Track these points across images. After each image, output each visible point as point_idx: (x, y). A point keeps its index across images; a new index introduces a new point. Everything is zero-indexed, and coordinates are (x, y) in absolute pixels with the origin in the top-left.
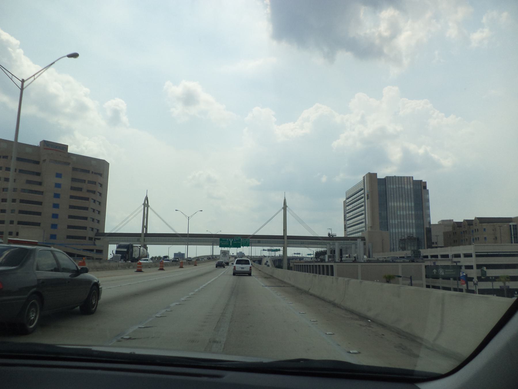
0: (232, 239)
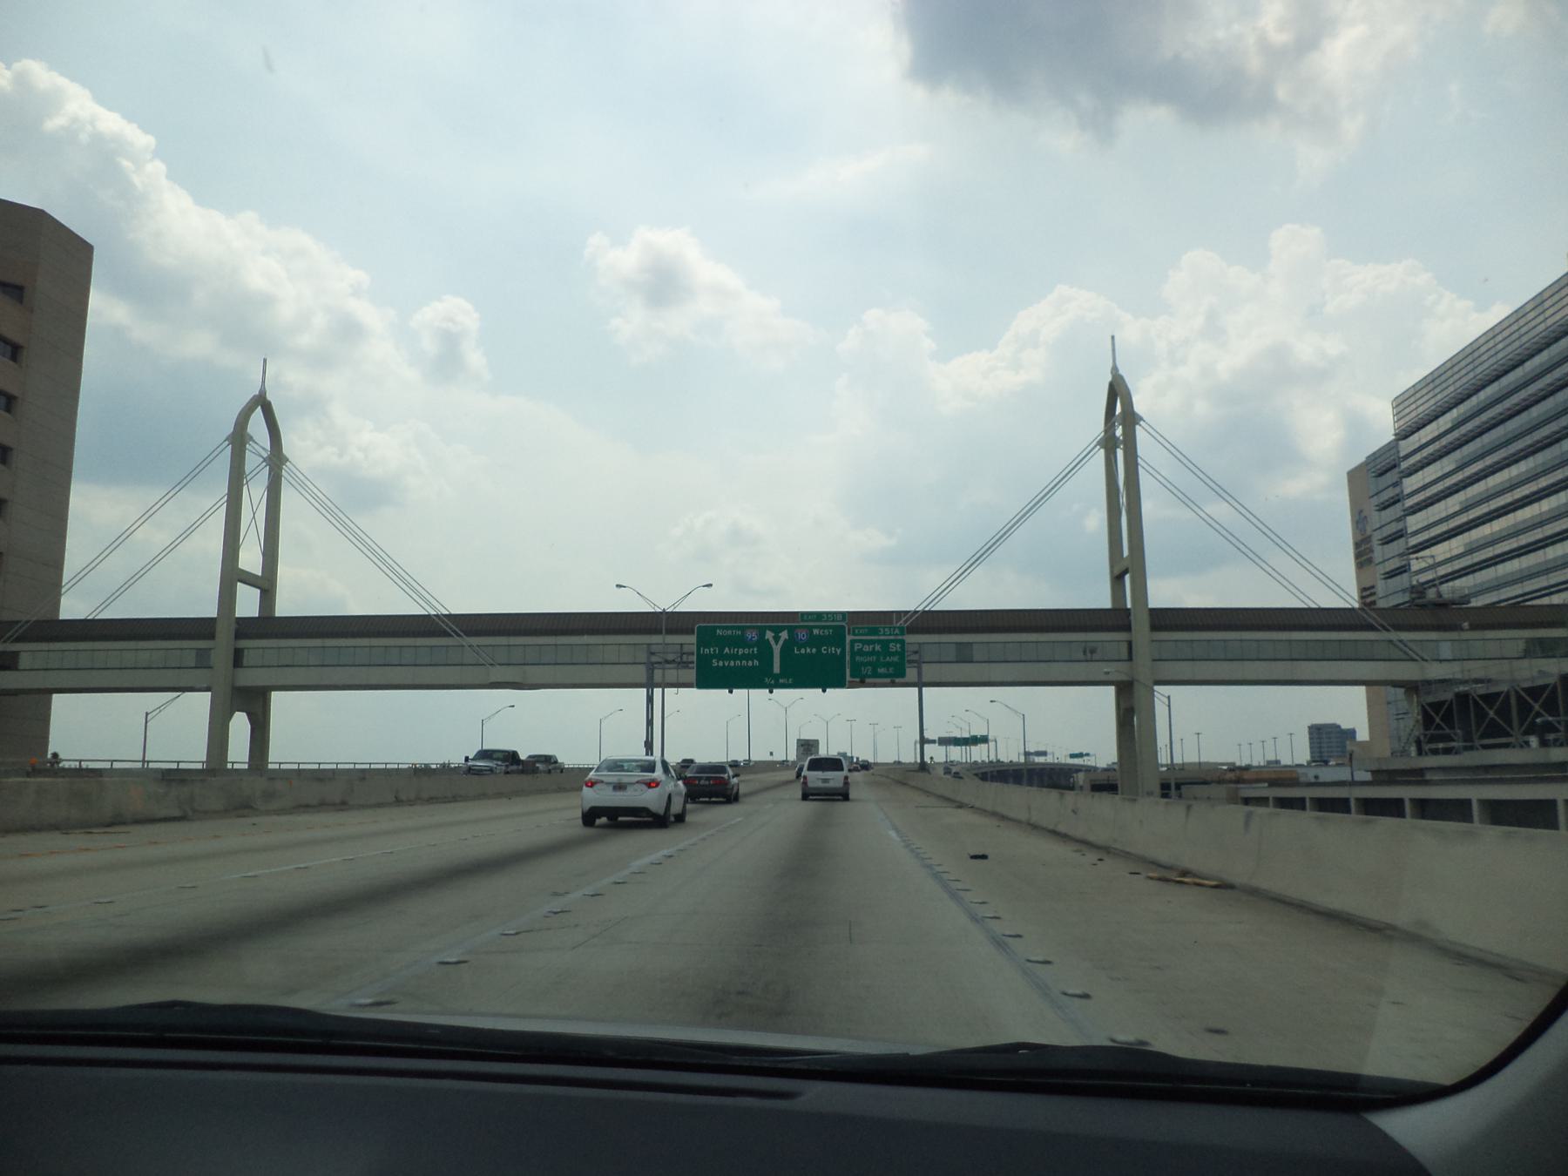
0: (781, 629)
